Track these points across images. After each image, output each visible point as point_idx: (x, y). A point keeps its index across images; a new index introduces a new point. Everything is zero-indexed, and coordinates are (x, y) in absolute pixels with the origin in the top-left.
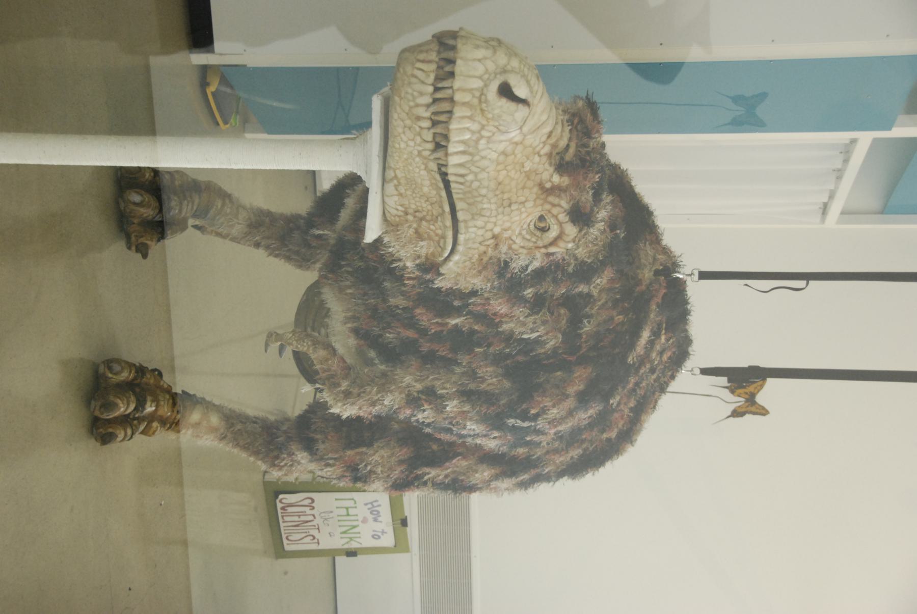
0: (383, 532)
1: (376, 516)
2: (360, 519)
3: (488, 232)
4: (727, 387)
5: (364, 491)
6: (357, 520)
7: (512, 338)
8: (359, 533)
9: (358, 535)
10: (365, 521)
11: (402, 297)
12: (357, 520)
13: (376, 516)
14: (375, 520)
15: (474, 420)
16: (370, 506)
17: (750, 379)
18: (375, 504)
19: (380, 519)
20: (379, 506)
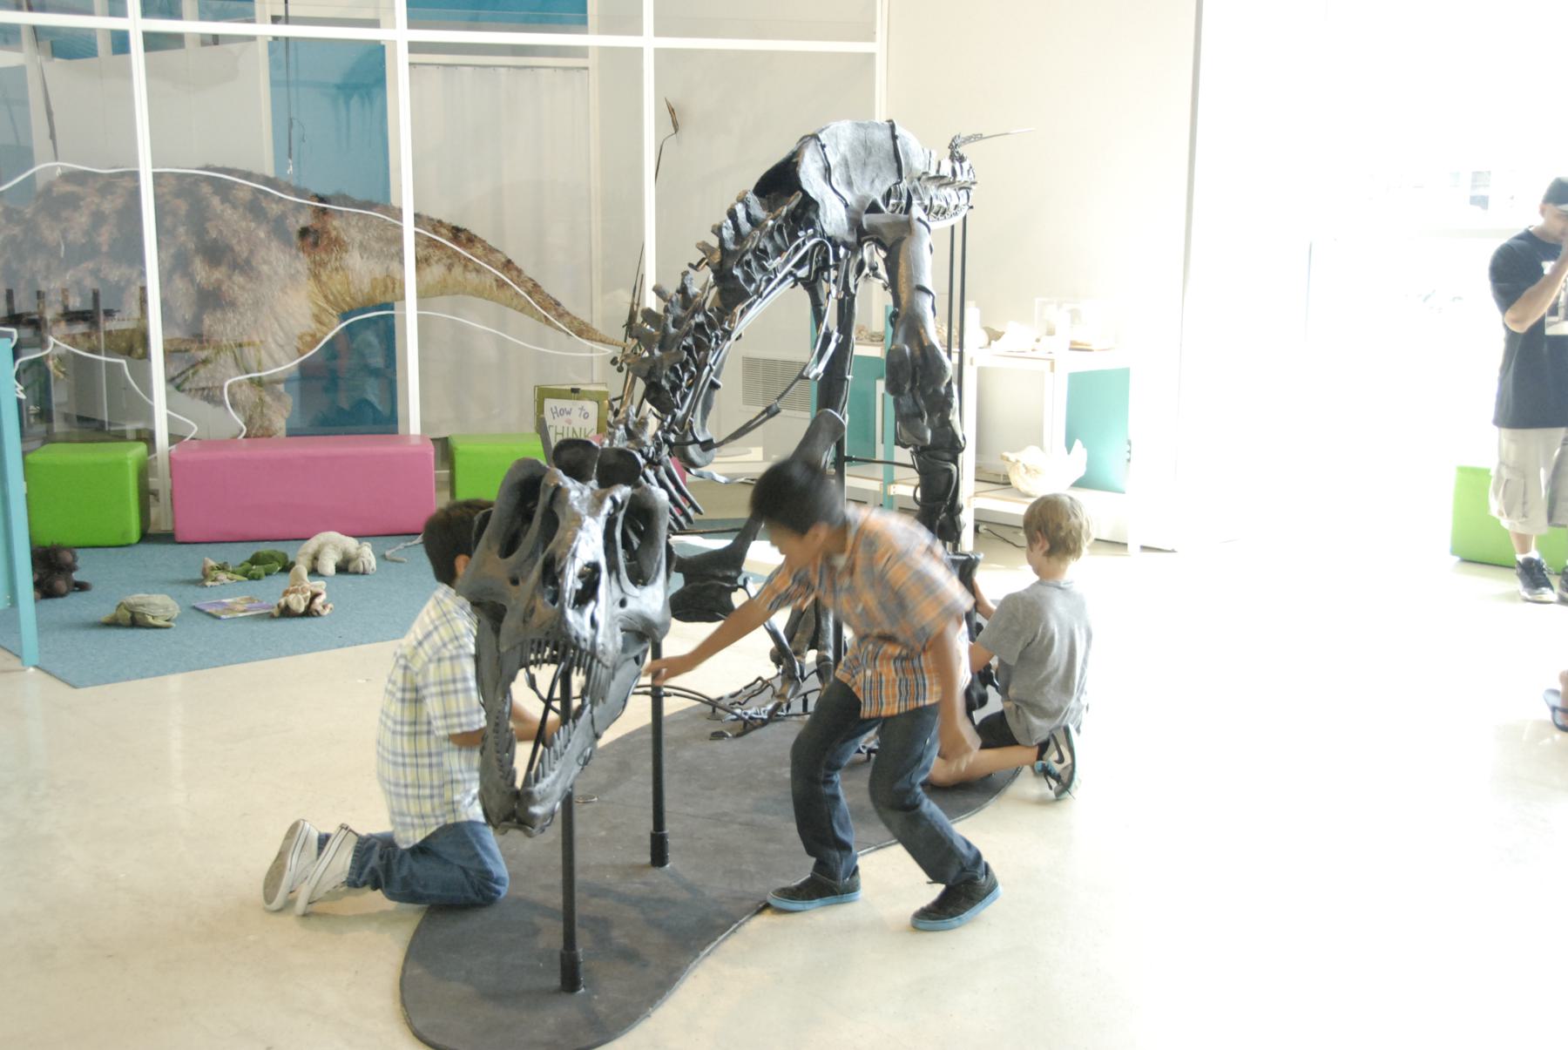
0: (582, 409)
1: (563, 412)
2: (567, 425)
3: (1081, 699)
4: (630, 595)
5: (805, 910)
6: (568, 428)
7: (569, 550)
8: (581, 429)
9: (583, 431)
10: (569, 422)
11: (33, 317)
12: (568, 428)
13: (563, 412)
14: (569, 413)
15: (842, 860)
16: (556, 415)
17: (511, 775)
18: (554, 410)
19: (568, 409)
20: (556, 408)
